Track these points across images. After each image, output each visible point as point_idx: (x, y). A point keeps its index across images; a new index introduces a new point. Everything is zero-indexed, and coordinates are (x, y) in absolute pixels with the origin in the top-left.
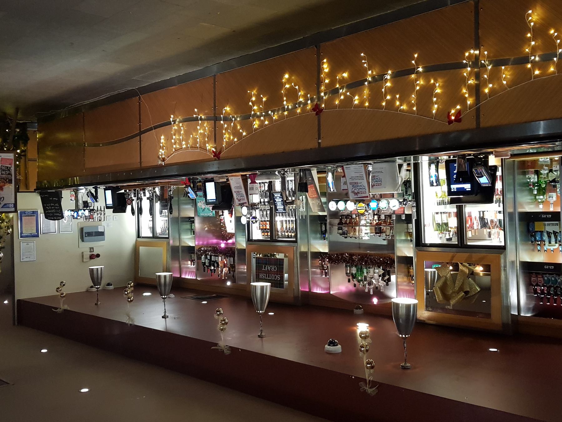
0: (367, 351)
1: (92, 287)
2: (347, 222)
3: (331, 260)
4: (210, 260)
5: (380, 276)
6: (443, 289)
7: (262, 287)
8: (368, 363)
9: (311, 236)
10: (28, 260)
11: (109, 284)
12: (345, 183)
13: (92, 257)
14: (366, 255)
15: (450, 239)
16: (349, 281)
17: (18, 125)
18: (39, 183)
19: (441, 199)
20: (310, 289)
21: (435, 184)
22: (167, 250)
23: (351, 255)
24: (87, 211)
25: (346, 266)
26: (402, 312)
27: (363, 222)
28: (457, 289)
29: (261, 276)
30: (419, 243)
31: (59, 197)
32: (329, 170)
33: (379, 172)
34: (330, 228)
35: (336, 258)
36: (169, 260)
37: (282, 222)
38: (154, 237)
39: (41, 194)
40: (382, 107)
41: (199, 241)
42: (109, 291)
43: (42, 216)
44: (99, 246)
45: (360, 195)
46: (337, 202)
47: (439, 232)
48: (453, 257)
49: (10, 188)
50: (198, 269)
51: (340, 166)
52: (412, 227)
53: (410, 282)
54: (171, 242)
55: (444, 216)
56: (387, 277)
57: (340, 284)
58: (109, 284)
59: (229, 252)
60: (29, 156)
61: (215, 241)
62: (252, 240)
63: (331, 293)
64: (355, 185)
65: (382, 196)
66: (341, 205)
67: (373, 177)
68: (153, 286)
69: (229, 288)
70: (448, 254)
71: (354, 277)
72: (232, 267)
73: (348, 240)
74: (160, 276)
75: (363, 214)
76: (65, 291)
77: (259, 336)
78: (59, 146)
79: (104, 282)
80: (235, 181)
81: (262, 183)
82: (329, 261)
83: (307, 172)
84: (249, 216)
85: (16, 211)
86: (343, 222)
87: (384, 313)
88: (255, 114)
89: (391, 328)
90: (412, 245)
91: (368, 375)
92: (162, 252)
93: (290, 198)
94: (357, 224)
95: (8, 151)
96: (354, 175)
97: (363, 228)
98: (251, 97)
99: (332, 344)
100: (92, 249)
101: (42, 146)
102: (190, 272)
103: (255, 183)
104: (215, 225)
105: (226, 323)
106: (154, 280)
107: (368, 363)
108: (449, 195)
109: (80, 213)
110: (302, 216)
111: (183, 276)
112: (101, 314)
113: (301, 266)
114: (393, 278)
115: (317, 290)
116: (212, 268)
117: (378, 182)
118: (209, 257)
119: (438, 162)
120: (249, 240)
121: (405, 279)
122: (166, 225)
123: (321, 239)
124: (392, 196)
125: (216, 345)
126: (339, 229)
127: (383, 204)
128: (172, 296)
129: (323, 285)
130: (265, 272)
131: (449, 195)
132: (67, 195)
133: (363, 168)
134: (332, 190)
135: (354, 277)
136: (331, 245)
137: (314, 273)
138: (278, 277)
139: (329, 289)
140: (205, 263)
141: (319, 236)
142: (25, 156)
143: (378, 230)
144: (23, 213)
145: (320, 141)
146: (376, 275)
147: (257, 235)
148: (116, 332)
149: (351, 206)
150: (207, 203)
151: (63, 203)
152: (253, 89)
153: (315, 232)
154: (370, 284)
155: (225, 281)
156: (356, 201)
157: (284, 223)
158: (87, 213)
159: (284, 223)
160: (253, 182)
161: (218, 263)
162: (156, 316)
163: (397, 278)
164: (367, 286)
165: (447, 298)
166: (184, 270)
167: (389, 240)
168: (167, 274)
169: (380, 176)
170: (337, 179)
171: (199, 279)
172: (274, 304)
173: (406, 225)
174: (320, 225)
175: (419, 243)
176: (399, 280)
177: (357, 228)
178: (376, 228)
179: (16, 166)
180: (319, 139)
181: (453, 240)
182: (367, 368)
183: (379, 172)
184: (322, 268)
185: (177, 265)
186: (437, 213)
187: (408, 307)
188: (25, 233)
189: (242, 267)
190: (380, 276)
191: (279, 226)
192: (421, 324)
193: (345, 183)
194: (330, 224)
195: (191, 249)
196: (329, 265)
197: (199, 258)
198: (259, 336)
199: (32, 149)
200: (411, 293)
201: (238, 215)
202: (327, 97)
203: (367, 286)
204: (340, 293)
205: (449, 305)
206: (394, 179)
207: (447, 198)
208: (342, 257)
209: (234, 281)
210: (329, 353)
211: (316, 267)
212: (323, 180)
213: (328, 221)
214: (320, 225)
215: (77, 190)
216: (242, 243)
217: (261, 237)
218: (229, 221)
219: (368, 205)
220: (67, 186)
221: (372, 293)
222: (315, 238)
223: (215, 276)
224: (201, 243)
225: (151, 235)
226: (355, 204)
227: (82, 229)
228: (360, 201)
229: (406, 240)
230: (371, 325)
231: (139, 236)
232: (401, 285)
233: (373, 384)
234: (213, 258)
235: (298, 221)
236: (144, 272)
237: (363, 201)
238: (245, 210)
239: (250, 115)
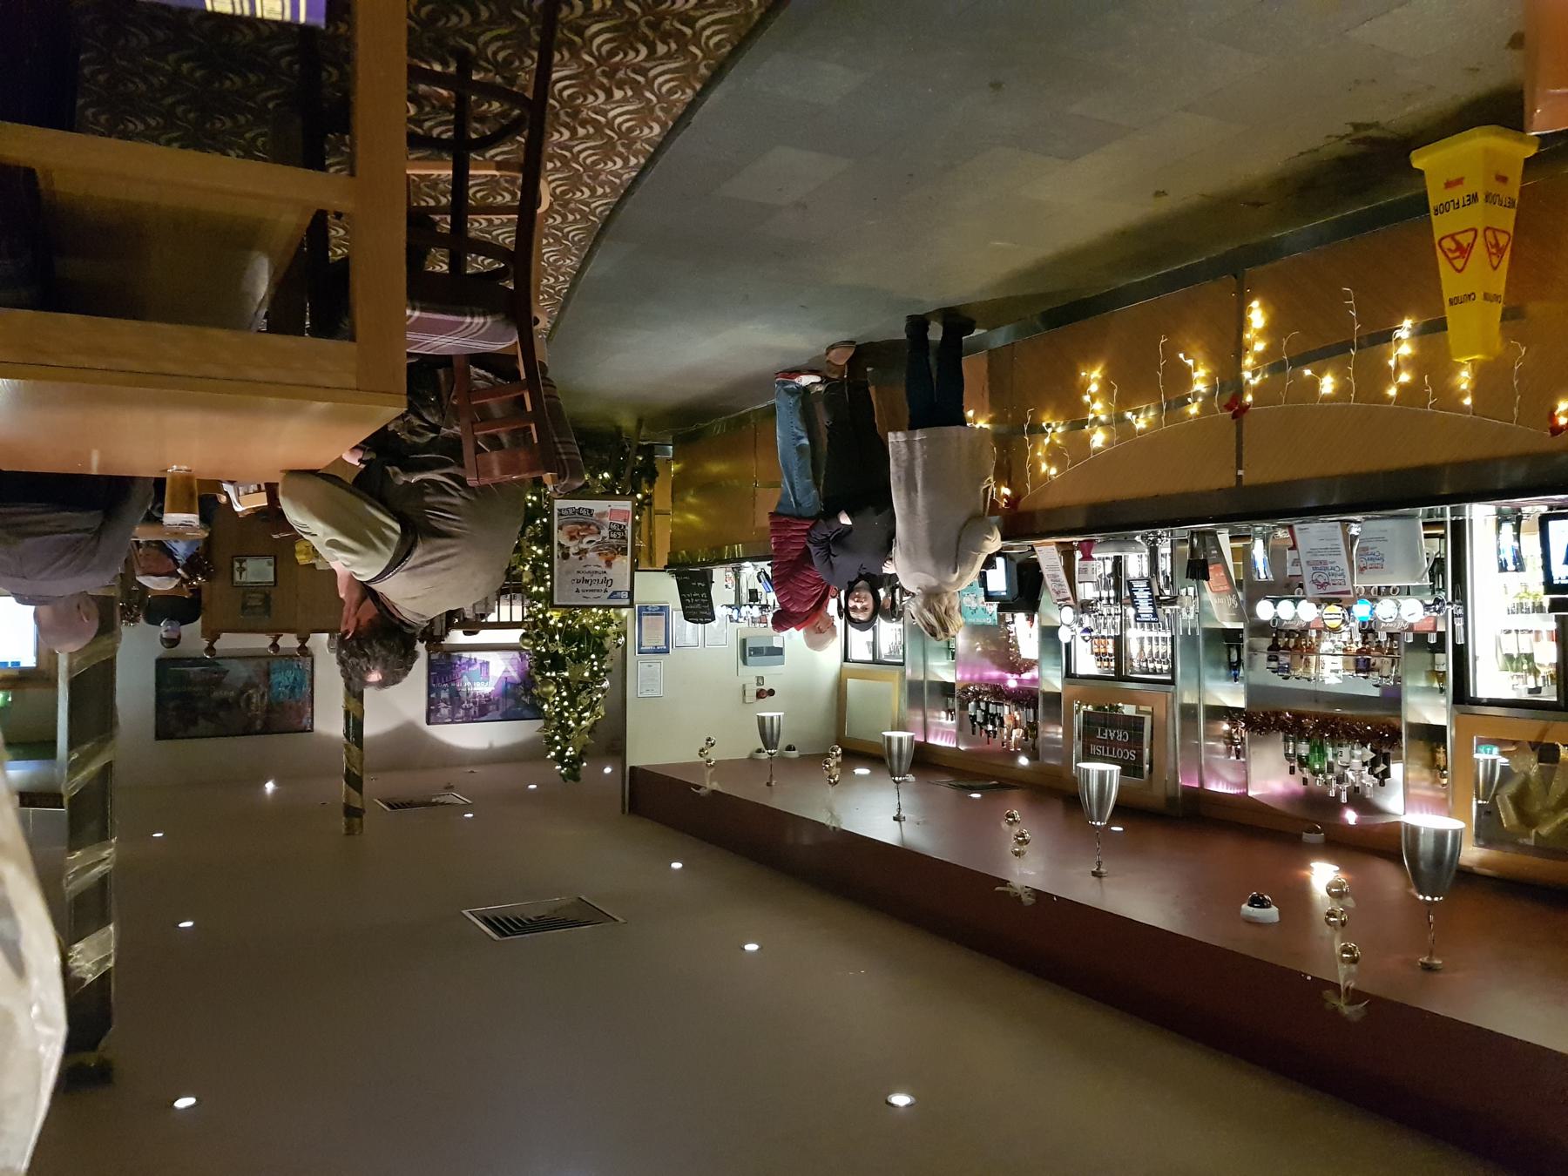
0: (1343, 924)
1: (759, 751)
2: (1290, 644)
3: (1252, 725)
4: (986, 711)
5: (1365, 764)
6: (1519, 800)
7: (1102, 775)
8: (1345, 950)
9: (1207, 672)
10: (650, 694)
11: (789, 748)
12: (1296, 562)
13: (760, 694)
14: (1334, 717)
15: (1537, 690)
16: (1292, 771)
17: (640, 449)
18: (673, 553)
19: (1517, 601)
20: (1202, 783)
21: (1511, 567)
22: (901, 689)
23: (1298, 716)
24: (756, 608)
25: (1286, 740)
26: (1426, 845)
27: (1325, 646)
28: (1552, 801)
29: (1093, 749)
30: (1462, 696)
31: (707, 580)
32: (1257, 535)
33: (1378, 539)
34: (1250, 658)
35: (1263, 719)
36: (904, 706)
37: (1142, 639)
38: (876, 661)
39: (678, 575)
40: (1388, 400)
41: (963, 673)
42: (790, 760)
43: (677, 616)
44: (773, 675)
45: (1329, 589)
46: (1275, 602)
47: (1510, 673)
48: (1544, 733)
49: (623, 563)
50: (960, 727)
51: (1283, 526)
52: (1446, 662)
53: (1436, 781)
54: (909, 672)
55: (1524, 638)
56: (1382, 767)
57: (1269, 776)
58: (789, 748)
59: (1026, 698)
60: (657, 505)
61: (995, 674)
62: (1074, 676)
63: (1251, 794)
64: (1319, 566)
65: (1387, 592)
66: (1286, 610)
67: (1362, 550)
68: (876, 757)
69: (1023, 769)
70: (1529, 728)
71: (1304, 762)
72: (1032, 729)
73: (1291, 684)
74: (889, 739)
75: (1335, 630)
76: (714, 755)
77: (1094, 874)
78: (709, 488)
79: (782, 743)
80: (1048, 555)
81: (1101, 563)
82: (1246, 728)
83: (1208, 539)
84: (1075, 626)
85: (631, 605)
86: (1281, 643)
87: (1380, 845)
88: (1096, 419)
89: (1390, 880)
90: (1444, 701)
91: (1343, 975)
92: (891, 692)
93: (1167, 592)
94: (1312, 650)
95: (623, 496)
96: (1316, 544)
97: (1327, 659)
98: (1089, 384)
99: (1258, 902)
100: (760, 680)
101: (680, 486)
102: (945, 734)
103: (1091, 558)
104: (995, 642)
105: (1026, 842)
106: (880, 746)
107: (1345, 950)
108: (1547, 592)
109: (744, 610)
110: (1185, 630)
111: (931, 741)
112: (777, 802)
113: (1182, 734)
114: (1396, 769)
115: (1216, 787)
116: (990, 727)
117: (1372, 561)
118: (983, 705)
119: (1519, 519)
120: (1069, 675)
121: (1426, 774)
122: (899, 638)
123: (1228, 678)
124: (1408, 591)
125: (1005, 883)
126: (1270, 660)
127: (1385, 609)
128: (911, 778)
129: (1231, 777)
130: (1103, 743)
131: (1547, 592)
132: (721, 576)
133: (1339, 530)
134: (1263, 576)
135: (1304, 762)
136: (1253, 692)
137: (1212, 750)
138: (1131, 755)
139: (1246, 785)
140: (974, 718)
141: (1223, 671)
142: (650, 504)
143: (1363, 666)
144: (644, 610)
145: (1240, 473)
146: (1356, 762)
147: (1086, 664)
148: (806, 840)
149: (1307, 612)
150: (989, 597)
151: (715, 591)
152: (1093, 367)
153: (1216, 664)
154: (1341, 779)
155: (1015, 755)
156: (1321, 602)
157: (1146, 642)
158: (756, 612)
159: (1146, 642)
160: (1087, 557)
161: (1001, 719)
162: (878, 814)
163: (1405, 771)
164: (1334, 784)
165: (1527, 819)
166: (933, 729)
167: (1385, 689)
168: (905, 735)
169: (1380, 548)
170: (1274, 555)
171: (962, 748)
172: (1123, 810)
173: (1429, 656)
174: (1226, 648)
175: (1462, 696)
176: (1410, 775)
177: (1313, 659)
178: (1357, 661)
179: (636, 524)
180: (1239, 467)
181: (1544, 692)
182: (1334, 959)
183: (1378, 539)
184: (1229, 739)
185: (919, 718)
186: (1509, 632)
187: (1440, 837)
188: (647, 645)
189: (1052, 729)
190: (1365, 764)
191: (1133, 649)
192: (1466, 876)
193: (1296, 562)
194: (1251, 649)
195: (947, 689)
196: (1245, 734)
197: (964, 707)
198: (1094, 874)
199: (662, 493)
200: (1441, 806)
201: (1047, 623)
202: (1258, 378)
203: (1334, 784)
204: (1271, 797)
205: (1528, 836)
206: (1413, 557)
207: (1546, 600)
208: (1277, 719)
209: (1034, 754)
210: (1251, 922)
211: (1218, 738)
212: (1244, 555)
213: (1246, 642)
214: (1226, 648)
215: (739, 569)
216: (1053, 680)
217: (1095, 671)
218: (1025, 634)
219: (1349, 610)
220: (721, 562)
221: (1344, 799)
222: (1217, 678)
223: (996, 744)
224: (967, 676)
225: (870, 658)
226: (1318, 606)
227: (744, 642)
228: (1329, 602)
229: (1430, 689)
230: (1344, 868)
231: (846, 659)
232: (1415, 787)
233: (1355, 996)
234: (992, 709)
235: (1178, 641)
236: (858, 728)
237: (1338, 602)
238: (1068, 614)
239: (1086, 422)
